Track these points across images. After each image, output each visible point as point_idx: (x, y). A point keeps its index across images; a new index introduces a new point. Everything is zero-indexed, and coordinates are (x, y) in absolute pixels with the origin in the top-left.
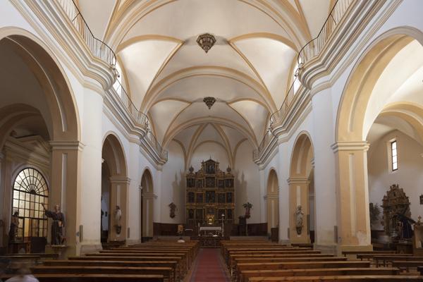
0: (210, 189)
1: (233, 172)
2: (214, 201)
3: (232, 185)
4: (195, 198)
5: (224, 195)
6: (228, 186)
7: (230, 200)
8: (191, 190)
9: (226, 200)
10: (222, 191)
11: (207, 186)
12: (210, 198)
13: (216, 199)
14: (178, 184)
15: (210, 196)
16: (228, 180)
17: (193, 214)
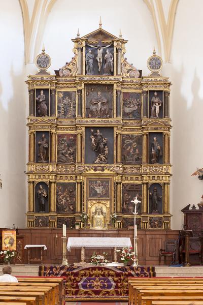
0: (98, 121)
1: (165, 71)
2: (110, 160)
3: (164, 111)
4: (55, 148)
5: (139, 140)
6: (150, 114)
7: (158, 157)
8: (43, 124)
9: (144, 160)
10: (133, 130)
11: (90, 113)
12: (98, 150)
13: (118, 153)
14: (6, 107)
15: (99, 144)
16: (152, 92)
17: (47, 198)
